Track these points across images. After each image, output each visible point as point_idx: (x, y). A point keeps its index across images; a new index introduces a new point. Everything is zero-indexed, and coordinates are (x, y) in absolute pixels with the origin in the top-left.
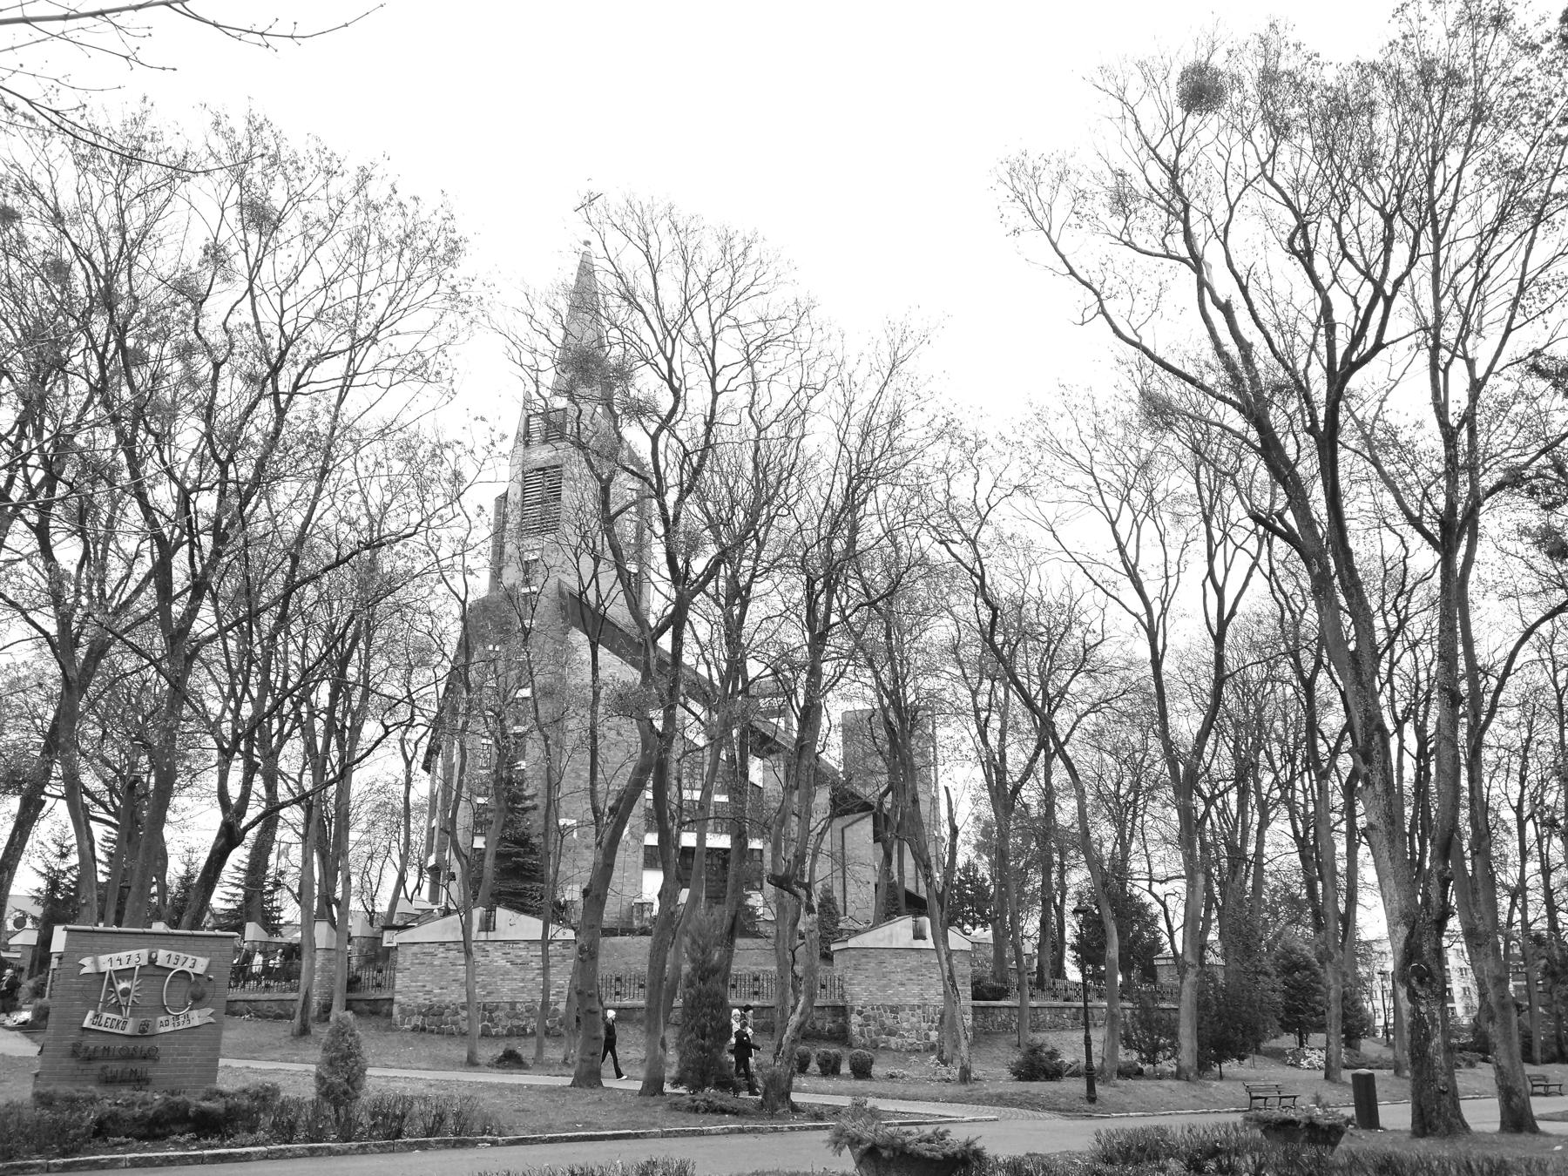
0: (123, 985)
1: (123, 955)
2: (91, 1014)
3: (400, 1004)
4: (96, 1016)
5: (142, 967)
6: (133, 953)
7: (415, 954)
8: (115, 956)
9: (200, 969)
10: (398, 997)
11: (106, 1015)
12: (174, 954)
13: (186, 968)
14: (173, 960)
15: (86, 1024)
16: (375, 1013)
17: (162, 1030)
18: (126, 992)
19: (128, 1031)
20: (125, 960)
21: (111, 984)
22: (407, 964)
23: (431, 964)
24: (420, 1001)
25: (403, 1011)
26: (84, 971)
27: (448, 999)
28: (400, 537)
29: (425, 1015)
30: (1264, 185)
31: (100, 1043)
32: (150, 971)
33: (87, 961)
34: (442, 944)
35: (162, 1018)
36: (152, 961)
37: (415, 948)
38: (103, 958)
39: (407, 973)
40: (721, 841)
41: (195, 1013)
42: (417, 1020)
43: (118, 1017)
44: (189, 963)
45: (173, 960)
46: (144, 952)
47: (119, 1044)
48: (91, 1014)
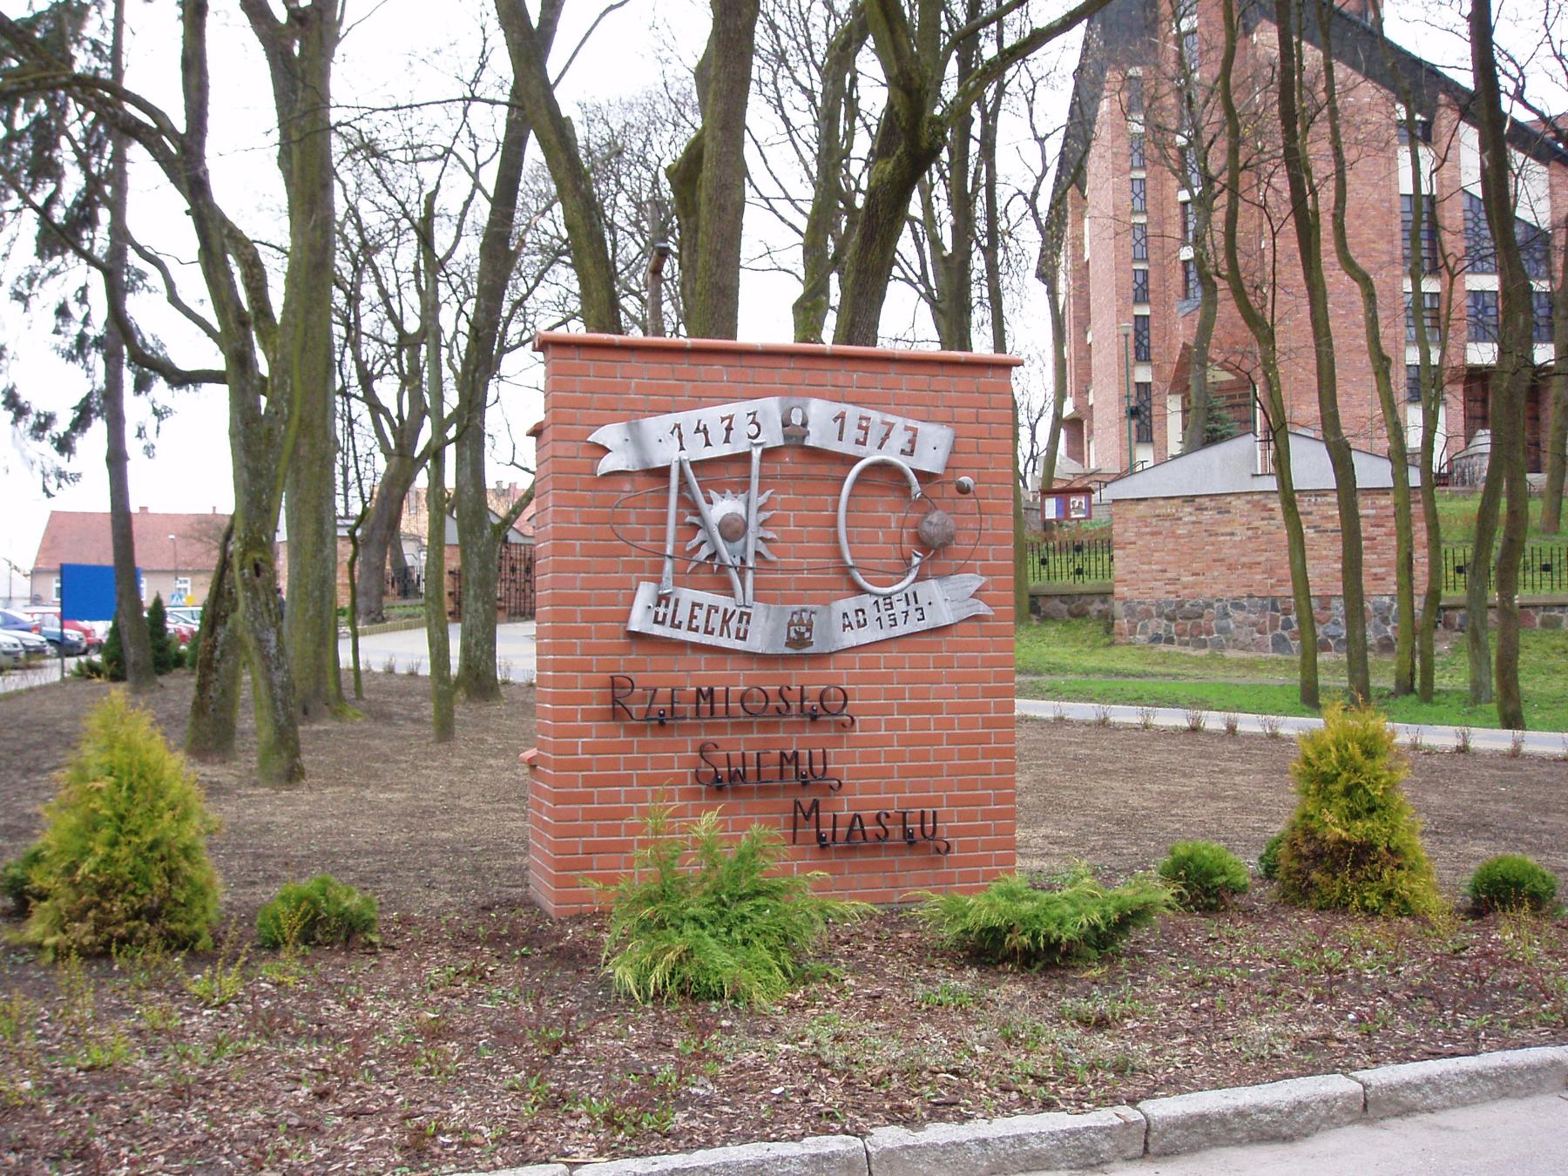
0: (723, 507)
1: (712, 415)
2: (645, 593)
3: (1125, 601)
4: (662, 599)
5: (768, 453)
6: (740, 409)
7: (1143, 520)
8: (688, 419)
9: (931, 458)
10: (1120, 590)
11: (688, 595)
12: (853, 412)
13: (891, 455)
14: (852, 432)
15: (639, 620)
16: (1080, 614)
17: (852, 638)
18: (733, 530)
19: (757, 642)
20: (717, 433)
21: (688, 503)
22: (1130, 536)
23: (1173, 535)
24: (1160, 595)
25: (1131, 612)
26: (607, 464)
27: (1207, 593)
28: (449, 255)
29: (1171, 619)
30: (1036, 75)
31: (691, 676)
32: (788, 460)
33: (609, 434)
34: (1190, 499)
35: (848, 604)
36: (795, 437)
37: (1142, 507)
38: (657, 426)
39: (1130, 549)
40: (1483, 354)
41: (932, 590)
42: (1158, 625)
43: (723, 601)
44: (898, 440)
45: (852, 432)
46: (771, 406)
47: (738, 680)
48: (645, 593)
